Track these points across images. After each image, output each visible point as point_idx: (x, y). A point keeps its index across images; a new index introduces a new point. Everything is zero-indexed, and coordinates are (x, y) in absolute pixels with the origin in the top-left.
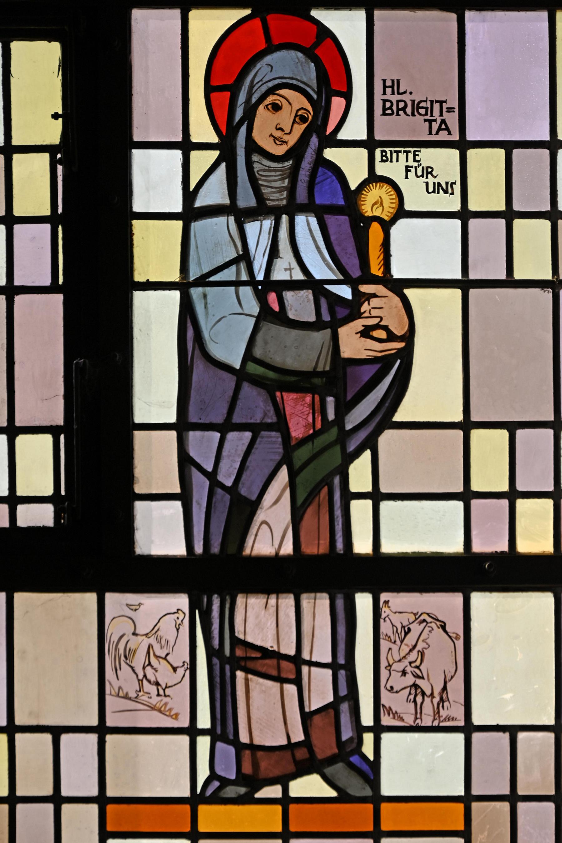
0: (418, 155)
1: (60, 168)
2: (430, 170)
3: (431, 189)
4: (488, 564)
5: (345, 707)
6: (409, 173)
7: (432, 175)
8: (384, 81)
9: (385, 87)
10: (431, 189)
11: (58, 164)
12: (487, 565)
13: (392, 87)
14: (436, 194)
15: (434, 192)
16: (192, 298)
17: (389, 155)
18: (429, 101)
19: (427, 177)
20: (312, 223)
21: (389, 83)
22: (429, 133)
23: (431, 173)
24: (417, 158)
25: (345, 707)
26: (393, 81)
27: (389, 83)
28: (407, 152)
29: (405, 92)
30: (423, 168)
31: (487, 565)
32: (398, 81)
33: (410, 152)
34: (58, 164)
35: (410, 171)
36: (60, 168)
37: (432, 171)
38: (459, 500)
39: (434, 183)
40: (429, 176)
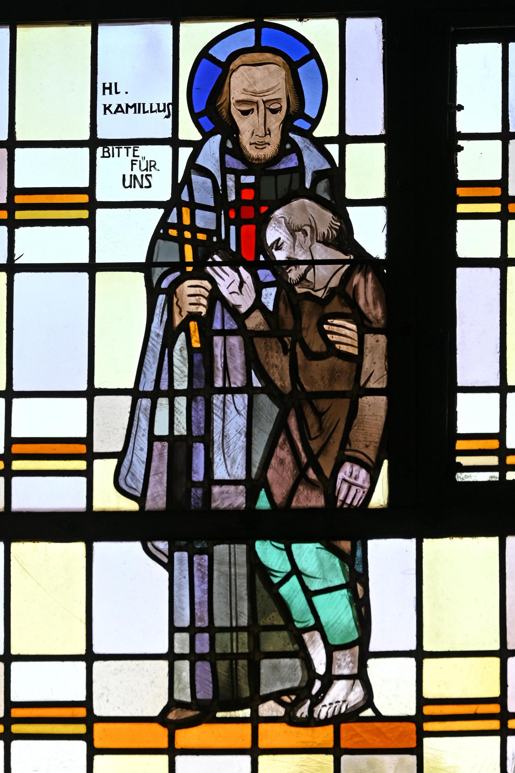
0: (137, 150)
1: (219, 715)
2: (153, 163)
3: (127, 184)
8: (104, 84)
9: (104, 88)
10: (127, 184)
11: (208, 261)
13: (110, 88)
15: (130, 186)
16: (288, 604)
17: (111, 152)
22: (458, 113)
23: (154, 166)
24: (136, 153)
26: (111, 84)
27: (107, 85)
28: (127, 148)
30: (147, 161)
32: (116, 84)
33: (130, 148)
34: (208, 261)
35: (135, 164)
36: (219, 715)
37: (155, 164)
38: (82, 660)
39: (131, 175)
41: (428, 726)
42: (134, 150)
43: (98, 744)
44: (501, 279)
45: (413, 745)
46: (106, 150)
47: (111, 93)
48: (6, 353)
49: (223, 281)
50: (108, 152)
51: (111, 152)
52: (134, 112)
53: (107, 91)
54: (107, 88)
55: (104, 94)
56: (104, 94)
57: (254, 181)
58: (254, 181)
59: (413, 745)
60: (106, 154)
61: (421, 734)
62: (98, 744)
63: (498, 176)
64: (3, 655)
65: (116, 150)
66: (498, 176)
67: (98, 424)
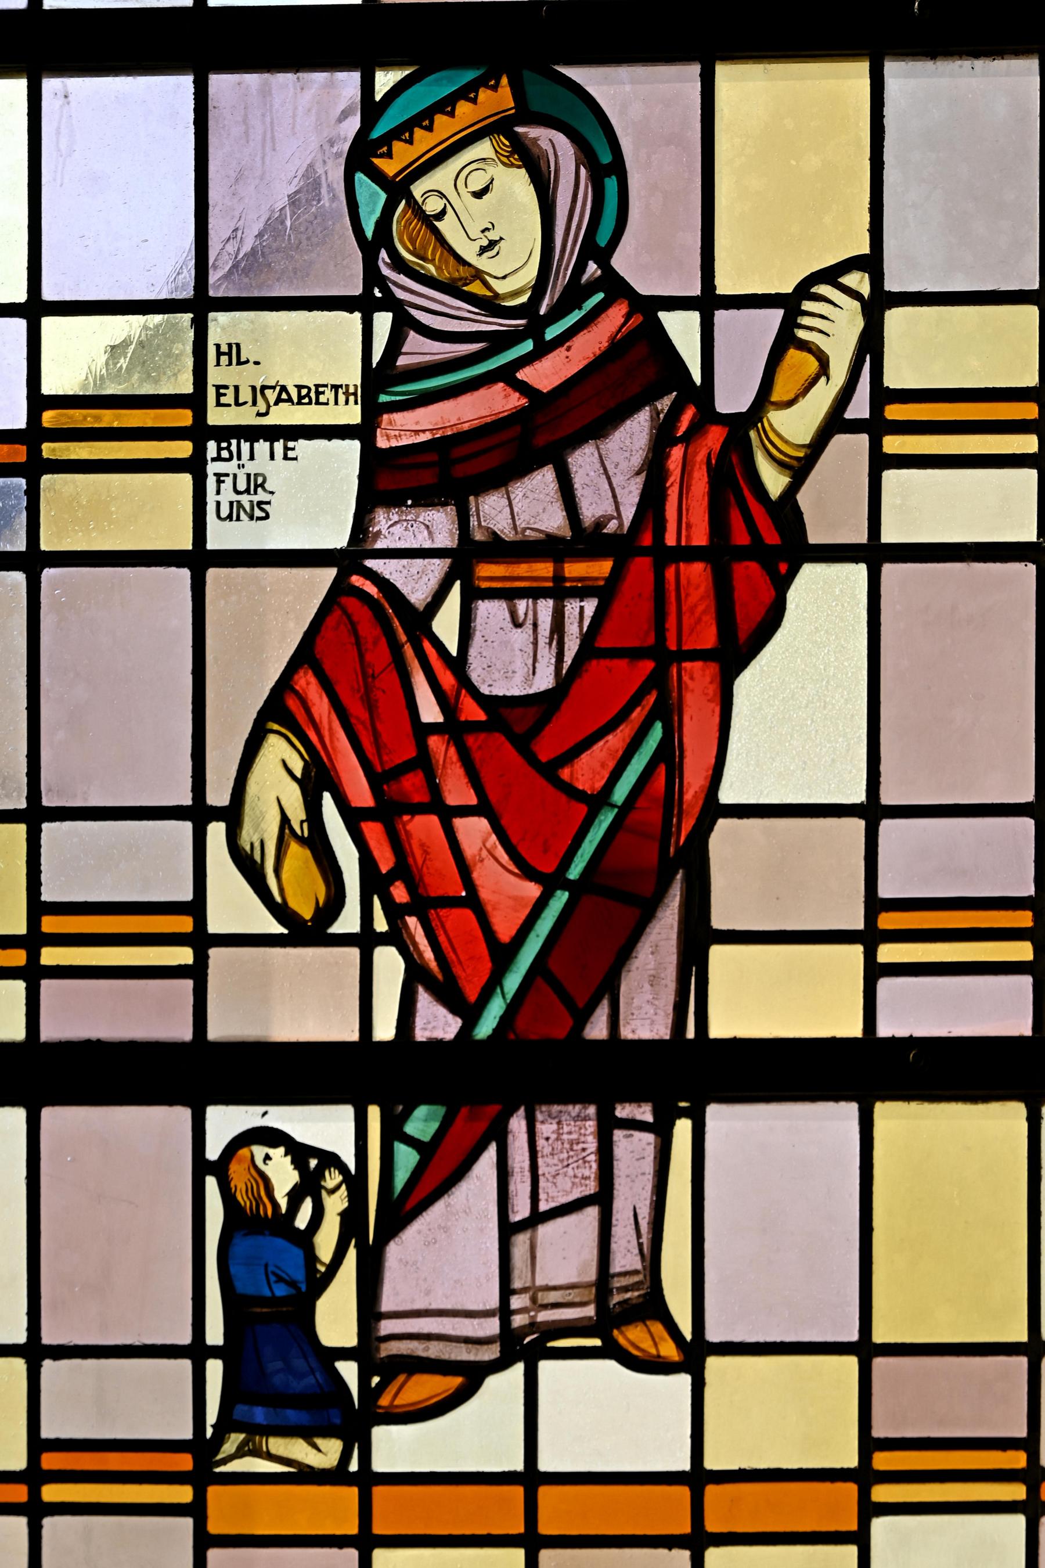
2: (260, 480)
4: (913, 1052)
5: (521, 1210)
6: (222, 485)
7: (264, 490)
8: (218, 346)
9: (219, 354)
12: (911, 1056)
13: (229, 354)
14: (234, 523)
15: (230, 517)
17: (234, 448)
18: (214, 386)
19: (256, 493)
20: (416, 512)
21: (224, 348)
23: (262, 485)
25: (521, 1210)
26: (230, 345)
29: (247, 362)
31: (911, 1056)
32: (238, 345)
37: (264, 481)
40: (259, 489)
41: (881, 1493)
42: (286, 449)
43: (214, 1527)
44: (879, 783)
45: (853, 1526)
46: (224, 445)
47: (230, 364)
48: (28, 95)
49: (280, 798)
50: (228, 448)
51: (234, 448)
52: (248, 458)
53: (224, 359)
54: (224, 354)
55: (218, 364)
56: (218, 364)
57: (804, 302)
58: (804, 302)
59: (853, 1526)
60: (225, 454)
61: (869, 1510)
62: (214, 1527)
63: (186, 894)
64: (24, 572)
65: (245, 447)
66: (186, 894)
67: (863, 680)
